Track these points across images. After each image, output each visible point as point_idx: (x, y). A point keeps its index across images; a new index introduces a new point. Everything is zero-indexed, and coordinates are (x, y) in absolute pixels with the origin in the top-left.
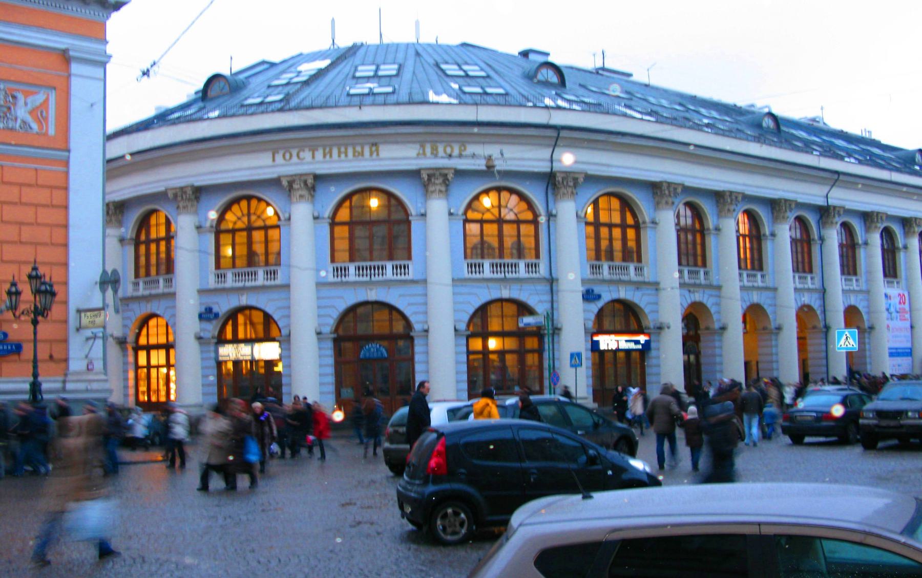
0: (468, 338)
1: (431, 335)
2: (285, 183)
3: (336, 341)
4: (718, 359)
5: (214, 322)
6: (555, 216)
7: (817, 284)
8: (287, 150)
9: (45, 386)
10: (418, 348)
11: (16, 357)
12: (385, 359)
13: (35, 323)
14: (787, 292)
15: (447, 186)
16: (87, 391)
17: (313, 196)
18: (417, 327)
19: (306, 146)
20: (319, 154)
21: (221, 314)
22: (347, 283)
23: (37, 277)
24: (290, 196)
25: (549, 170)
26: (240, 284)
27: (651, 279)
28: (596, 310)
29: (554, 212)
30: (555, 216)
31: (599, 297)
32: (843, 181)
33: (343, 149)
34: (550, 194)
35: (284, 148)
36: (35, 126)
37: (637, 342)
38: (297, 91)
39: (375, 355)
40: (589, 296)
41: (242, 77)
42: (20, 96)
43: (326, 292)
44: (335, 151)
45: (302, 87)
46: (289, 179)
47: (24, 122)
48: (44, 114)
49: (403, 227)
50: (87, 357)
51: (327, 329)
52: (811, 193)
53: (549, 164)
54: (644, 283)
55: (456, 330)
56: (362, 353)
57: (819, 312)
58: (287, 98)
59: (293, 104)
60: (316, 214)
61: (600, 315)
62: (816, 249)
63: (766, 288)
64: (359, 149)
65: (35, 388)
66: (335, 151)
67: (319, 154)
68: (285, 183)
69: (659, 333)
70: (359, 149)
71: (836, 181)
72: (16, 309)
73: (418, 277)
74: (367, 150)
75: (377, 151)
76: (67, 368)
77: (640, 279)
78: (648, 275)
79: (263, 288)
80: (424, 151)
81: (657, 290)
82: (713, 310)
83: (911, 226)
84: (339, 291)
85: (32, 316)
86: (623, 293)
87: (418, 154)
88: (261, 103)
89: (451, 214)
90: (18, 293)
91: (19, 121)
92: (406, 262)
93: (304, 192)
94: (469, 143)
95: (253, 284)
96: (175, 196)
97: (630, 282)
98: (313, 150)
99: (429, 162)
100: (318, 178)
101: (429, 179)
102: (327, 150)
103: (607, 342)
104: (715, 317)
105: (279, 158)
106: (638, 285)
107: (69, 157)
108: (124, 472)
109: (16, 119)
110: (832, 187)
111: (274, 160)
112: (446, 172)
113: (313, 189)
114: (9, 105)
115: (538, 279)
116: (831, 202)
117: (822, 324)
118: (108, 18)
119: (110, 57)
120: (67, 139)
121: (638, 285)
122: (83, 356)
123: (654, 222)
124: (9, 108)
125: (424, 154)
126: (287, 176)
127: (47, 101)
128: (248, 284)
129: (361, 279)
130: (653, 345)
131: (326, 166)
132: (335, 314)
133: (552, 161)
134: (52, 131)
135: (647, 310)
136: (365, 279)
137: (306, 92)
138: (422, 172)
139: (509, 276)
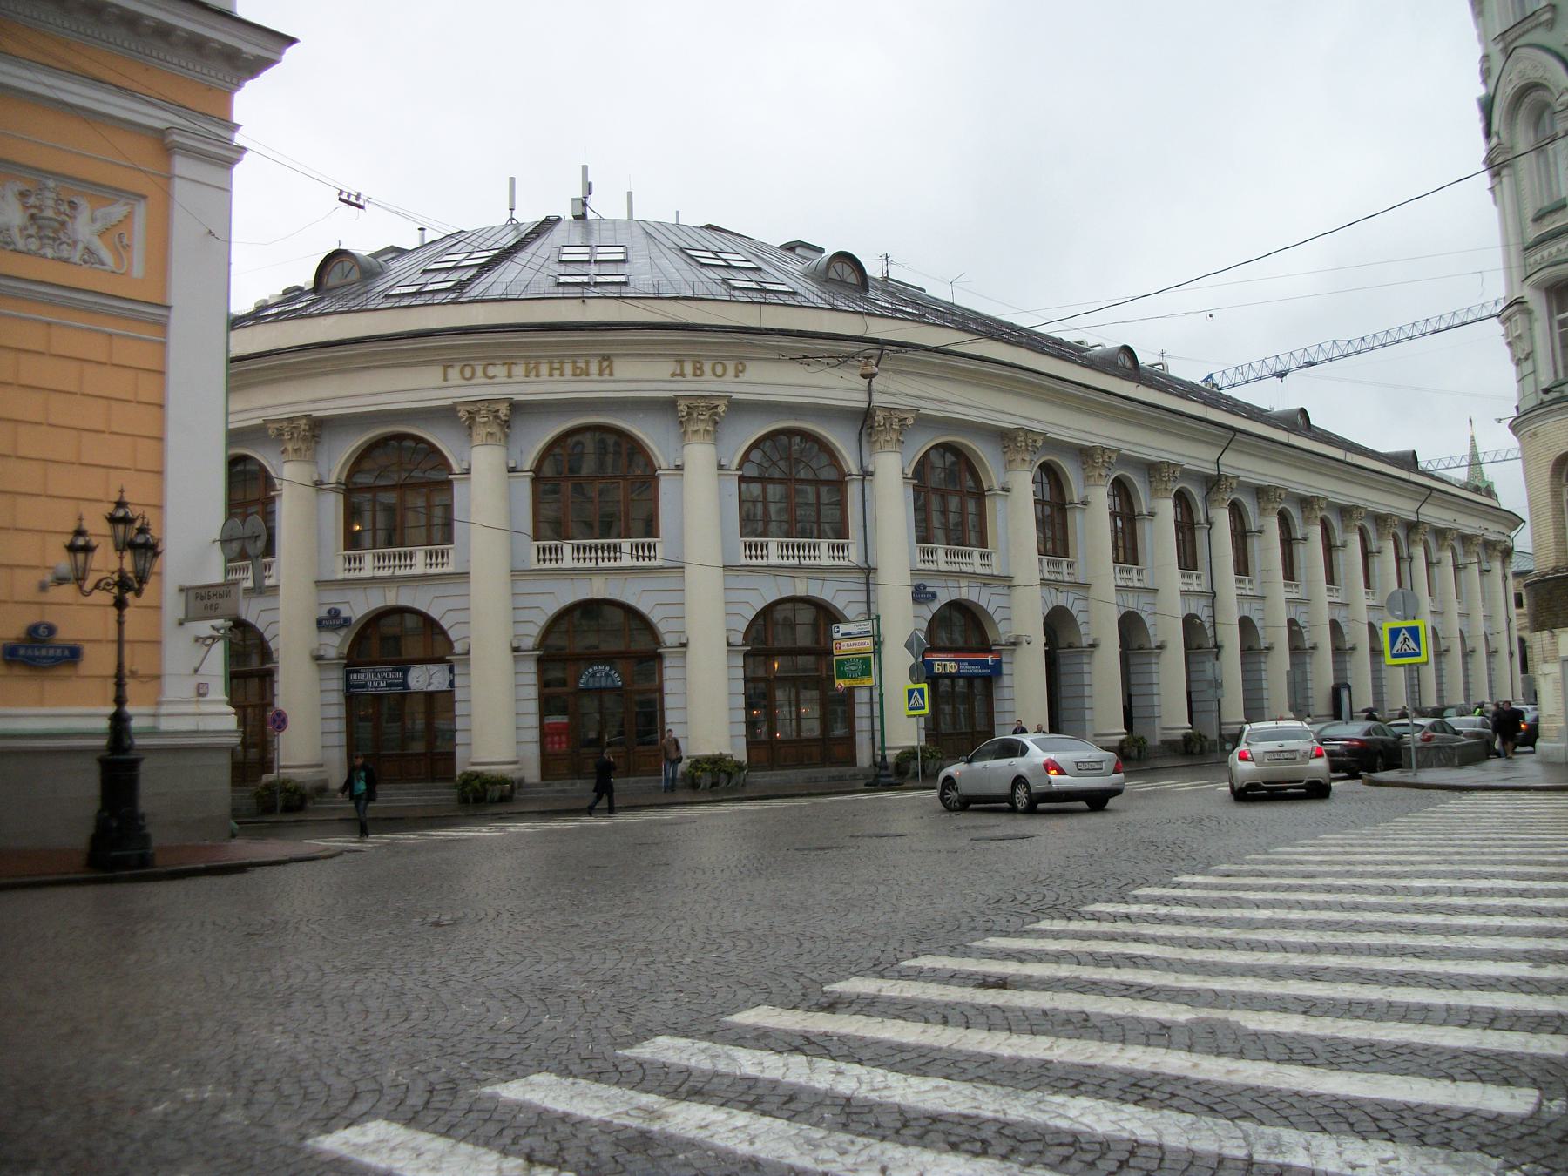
1: (692, 650)
2: (463, 414)
3: (540, 661)
4: (1087, 689)
5: (343, 632)
6: (872, 474)
7: (1205, 587)
8: (467, 363)
9: (135, 724)
12: (619, 688)
13: (120, 604)
14: (1170, 596)
18: (669, 640)
23: (127, 521)
24: (470, 435)
26: (387, 573)
28: (772, 597)
29: (871, 469)
30: (872, 474)
31: (934, 596)
36: (106, 255)
37: (984, 664)
39: (603, 684)
40: (921, 595)
41: (380, 260)
44: (544, 369)
47: (88, 250)
51: (529, 642)
52: (1198, 457)
53: (865, 397)
55: (729, 644)
57: (1207, 625)
60: (512, 464)
61: (936, 623)
62: (1201, 536)
65: (119, 721)
67: (519, 370)
68: (463, 414)
74: (594, 368)
75: (610, 366)
76: (160, 691)
77: (987, 571)
79: (425, 577)
82: (1080, 619)
84: (548, 584)
86: (966, 592)
87: (673, 375)
89: (721, 467)
90: (88, 549)
91: (80, 246)
93: (495, 429)
95: (408, 572)
96: (280, 432)
97: (973, 575)
98: (509, 363)
100: (516, 407)
103: (945, 665)
104: (1083, 629)
105: (454, 374)
106: (987, 580)
109: (74, 244)
111: (445, 379)
113: (507, 424)
117: (1211, 643)
118: (239, 86)
119: (242, 150)
124: (63, 224)
130: (1005, 669)
131: (533, 388)
132: (542, 620)
134: (138, 271)
135: (996, 618)
137: (489, 278)
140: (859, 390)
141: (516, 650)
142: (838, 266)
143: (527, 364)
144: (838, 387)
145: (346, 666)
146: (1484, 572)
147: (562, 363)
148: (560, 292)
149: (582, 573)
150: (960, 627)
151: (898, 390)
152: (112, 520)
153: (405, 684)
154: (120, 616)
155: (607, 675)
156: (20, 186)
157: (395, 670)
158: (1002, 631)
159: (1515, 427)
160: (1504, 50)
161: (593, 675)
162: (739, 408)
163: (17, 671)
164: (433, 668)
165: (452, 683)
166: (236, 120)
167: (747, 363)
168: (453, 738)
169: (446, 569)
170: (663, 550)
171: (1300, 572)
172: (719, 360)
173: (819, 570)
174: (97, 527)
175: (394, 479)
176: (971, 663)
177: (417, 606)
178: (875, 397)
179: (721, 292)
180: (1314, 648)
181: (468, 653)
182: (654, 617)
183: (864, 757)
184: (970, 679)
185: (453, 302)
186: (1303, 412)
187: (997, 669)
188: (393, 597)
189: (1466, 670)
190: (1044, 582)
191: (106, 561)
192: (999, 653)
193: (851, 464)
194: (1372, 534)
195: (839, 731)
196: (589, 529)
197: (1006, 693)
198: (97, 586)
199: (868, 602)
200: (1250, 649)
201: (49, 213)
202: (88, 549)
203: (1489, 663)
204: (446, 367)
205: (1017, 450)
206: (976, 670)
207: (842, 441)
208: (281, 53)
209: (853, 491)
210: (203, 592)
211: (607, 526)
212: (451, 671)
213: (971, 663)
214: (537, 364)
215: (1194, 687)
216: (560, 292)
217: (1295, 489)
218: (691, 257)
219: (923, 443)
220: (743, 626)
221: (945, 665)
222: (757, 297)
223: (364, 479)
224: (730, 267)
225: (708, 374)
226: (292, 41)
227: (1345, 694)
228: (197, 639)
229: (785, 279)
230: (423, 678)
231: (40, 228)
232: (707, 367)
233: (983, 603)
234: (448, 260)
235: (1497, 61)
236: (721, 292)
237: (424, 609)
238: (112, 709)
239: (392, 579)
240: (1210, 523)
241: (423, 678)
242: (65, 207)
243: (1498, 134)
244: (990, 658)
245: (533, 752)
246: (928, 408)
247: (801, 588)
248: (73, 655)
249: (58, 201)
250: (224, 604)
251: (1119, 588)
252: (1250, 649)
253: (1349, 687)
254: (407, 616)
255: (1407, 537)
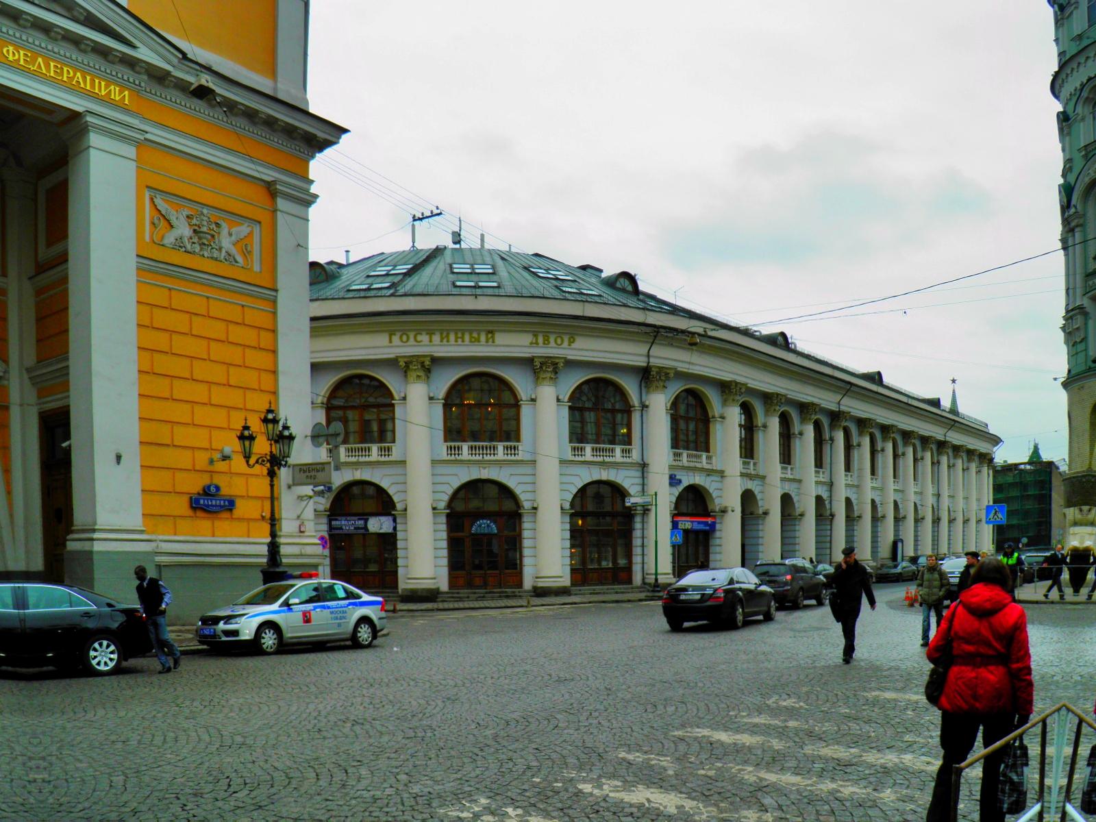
0: (572, 516)
1: (540, 513)
3: (448, 516)
6: (647, 407)
8: (404, 332)
10: (526, 524)
11: (225, 515)
15: (556, 373)
16: (301, 555)
17: (428, 378)
18: (527, 505)
19: (423, 330)
20: (436, 338)
21: (334, 488)
22: (462, 462)
24: (406, 376)
25: (645, 365)
26: (354, 459)
27: (719, 469)
28: (588, 480)
29: (647, 403)
30: (647, 407)
31: (680, 481)
32: (853, 391)
33: (460, 335)
34: (643, 388)
35: (415, 330)
36: (239, 259)
37: (706, 524)
38: (401, 281)
39: (486, 532)
40: (674, 481)
42: (224, 225)
43: (441, 469)
44: (452, 337)
45: (404, 277)
46: (405, 360)
48: (249, 249)
49: (513, 411)
50: (298, 517)
51: (442, 505)
53: (645, 359)
54: (712, 470)
55: (562, 509)
56: (473, 529)
57: (826, 502)
58: (393, 285)
59: (401, 291)
61: (680, 499)
63: (794, 480)
64: (475, 335)
66: (452, 337)
67: (436, 338)
68: (402, 364)
69: (723, 516)
70: (475, 335)
71: (848, 390)
72: (249, 457)
73: (528, 457)
74: (483, 338)
75: (493, 337)
78: (717, 464)
79: (378, 463)
80: (537, 340)
81: (722, 477)
82: (759, 497)
83: (888, 432)
84: (452, 469)
85: (268, 465)
86: (698, 480)
87: (531, 343)
88: (369, 289)
89: (431, 398)
91: (224, 251)
92: (516, 444)
93: (421, 373)
94: (577, 335)
95: (367, 459)
97: (702, 470)
98: (431, 333)
99: (540, 351)
100: (435, 360)
101: (541, 367)
102: (444, 335)
104: (760, 503)
105: (396, 339)
106: (709, 472)
107: (276, 297)
108: (913, 609)
109: (220, 249)
110: (845, 395)
111: (391, 342)
112: (557, 361)
113: (428, 371)
114: (212, 232)
115: (631, 463)
116: (843, 408)
117: (828, 512)
118: (313, 157)
119: (316, 196)
120: (274, 279)
121: (709, 472)
122: (295, 516)
123: (723, 417)
124: (213, 236)
125: (537, 343)
126: (405, 357)
127: (250, 234)
128: (362, 459)
129: (474, 458)
130: (718, 526)
131: (445, 349)
133: (648, 356)
135: (714, 495)
136: (478, 458)
138: (536, 360)
139: (607, 459)
140: (631, 357)
141: (434, 509)
142: (622, 280)
143: (441, 334)
144: (630, 353)
145: (329, 516)
146: (978, 472)
147: (463, 334)
148: (455, 291)
149: (474, 464)
150: (694, 501)
151: (665, 356)
152: (265, 421)
153: (366, 528)
154: (272, 481)
155: (488, 526)
156: (186, 212)
157: (359, 519)
158: (717, 503)
159: (1065, 385)
160: (1085, 156)
161: (480, 526)
162: (571, 364)
163: (199, 513)
164: (383, 519)
165: (395, 528)
166: (311, 178)
167: (576, 337)
168: (396, 563)
169: (391, 458)
170: (396, 455)
171: (880, 471)
172: (560, 335)
173: (494, 464)
174: (256, 425)
175: (357, 402)
176: (699, 523)
177: (374, 480)
178: (652, 360)
179: (556, 293)
180: (859, 517)
181: (406, 510)
182: (518, 490)
183: (637, 579)
184: (697, 532)
185: (392, 295)
186: (879, 374)
187: (713, 527)
188: (359, 475)
189: (916, 531)
190: (742, 475)
191: (262, 446)
192: (714, 517)
193: (635, 399)
194: (919, 448)
195: (622, 562)
196: (475, 436)
197: (718, 542)
198: (257, 462)
199: (643, 485)
200: (821, 515)
201: (204, 229)
202: (252, 438)
203: (949, 527)
204: (390, 336)
205: (730, 392)
206: (701, 527)
207: (631, 387)
208: (339, 138)
209: (636, 417)
210: (305, 468)
211: (365, 436)
212: (395, 521)
213: (699, 523)
214: (448, 334)
215: (747, 542)
216: (455, 291)
217: (881, 420)
218: (533, 272)
219: (675, 388)
220: (570, 497)
221: (686, 524)
222: (579, 298)
223: (338, 402)
224: (557, 279)
225: (552, 344)
226: (345, 131)
227: (900, 545)
228: (299, 497)
229: (592, 288)
230: (378, 525)
231: (200, 238)
232: (552, 339)
233: (707, 486)
234: (381, 270)
235: (1079, 163)
236: (556, 293)
237: (590, 480)
238: (268, 540)
239: (358, 464)
240: (832, 439)
241: (378, 525)
242: (213, 226)
243: (1075, 207)
244: (710, 520)
245: (444, 573)
246: (682, 367)
247: (604, 475)
248: (230, 505)
249: (209, 222)
250: (321, 476)
251: (783, 480)
252: (821, 515)
253: (902, 541)
254: (367, 487)
255: (938, 450)
